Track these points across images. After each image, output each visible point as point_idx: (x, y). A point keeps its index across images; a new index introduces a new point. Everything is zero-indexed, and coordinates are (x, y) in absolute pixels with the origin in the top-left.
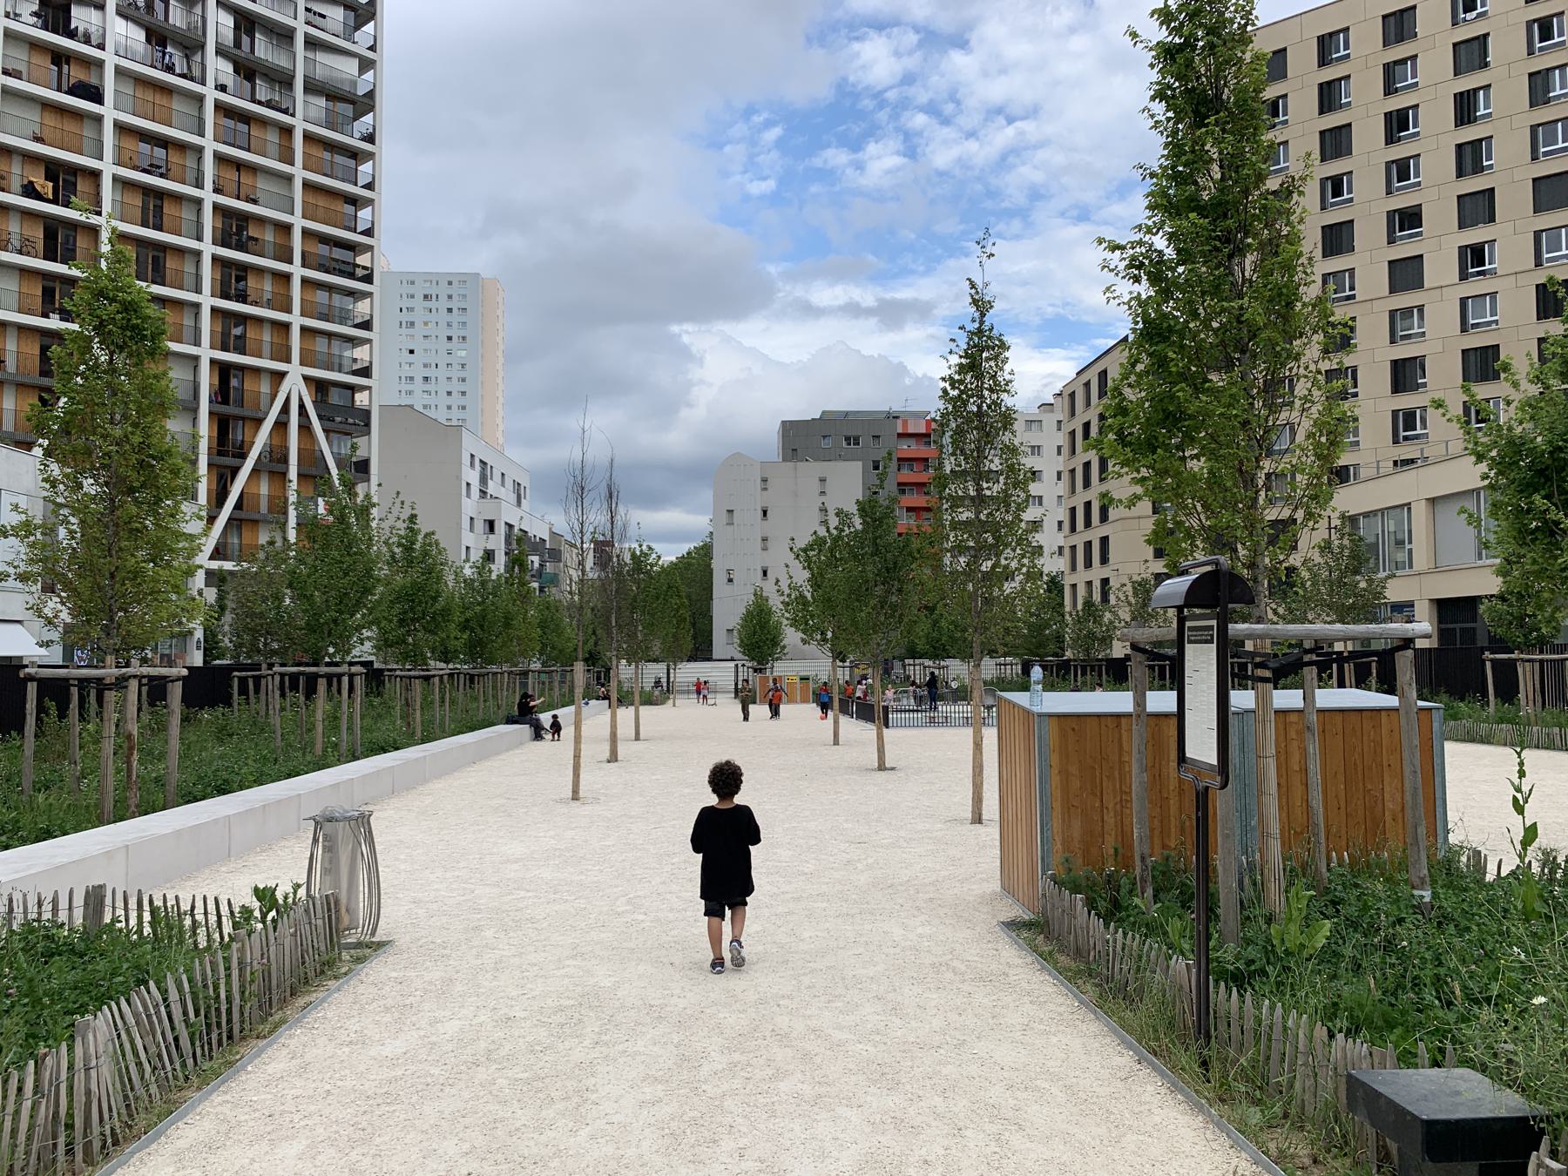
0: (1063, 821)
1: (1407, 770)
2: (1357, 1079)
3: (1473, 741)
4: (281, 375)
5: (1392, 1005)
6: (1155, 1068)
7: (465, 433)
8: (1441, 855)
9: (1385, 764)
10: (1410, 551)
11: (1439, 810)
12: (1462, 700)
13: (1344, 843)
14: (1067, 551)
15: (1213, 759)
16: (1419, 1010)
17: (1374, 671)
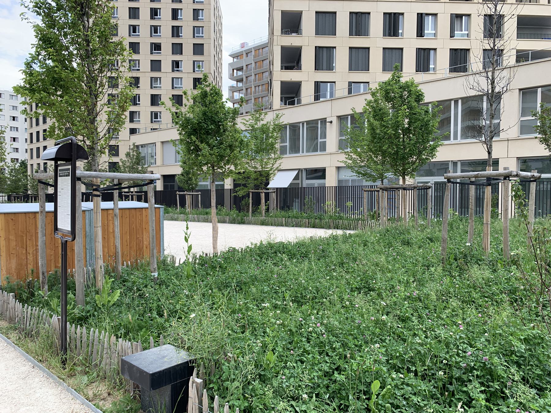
0: (7, 261)
1: (151, 229)
2: (125, 361)
3: (172, 220)
5: (142, 320)
6: (40, 369)
8: (161, 259)
9: (144, 227)
10: (155, 158)
11: (161, 243)
12: (170, 207)
13: (129, 258)
14: (29, 151)
15: (69, 229)
16: (152, 320)
17: (143, 198)
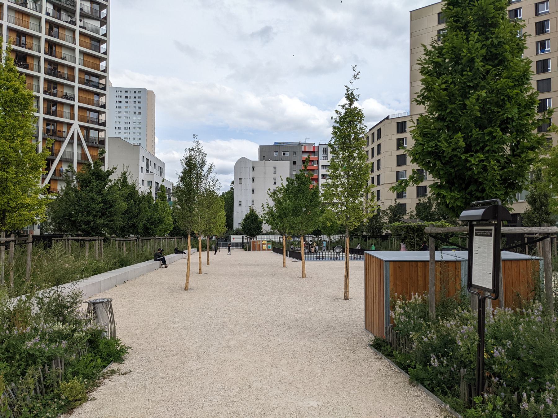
4: (70, 125)
7: (141, 149)
15: (490, 286)
